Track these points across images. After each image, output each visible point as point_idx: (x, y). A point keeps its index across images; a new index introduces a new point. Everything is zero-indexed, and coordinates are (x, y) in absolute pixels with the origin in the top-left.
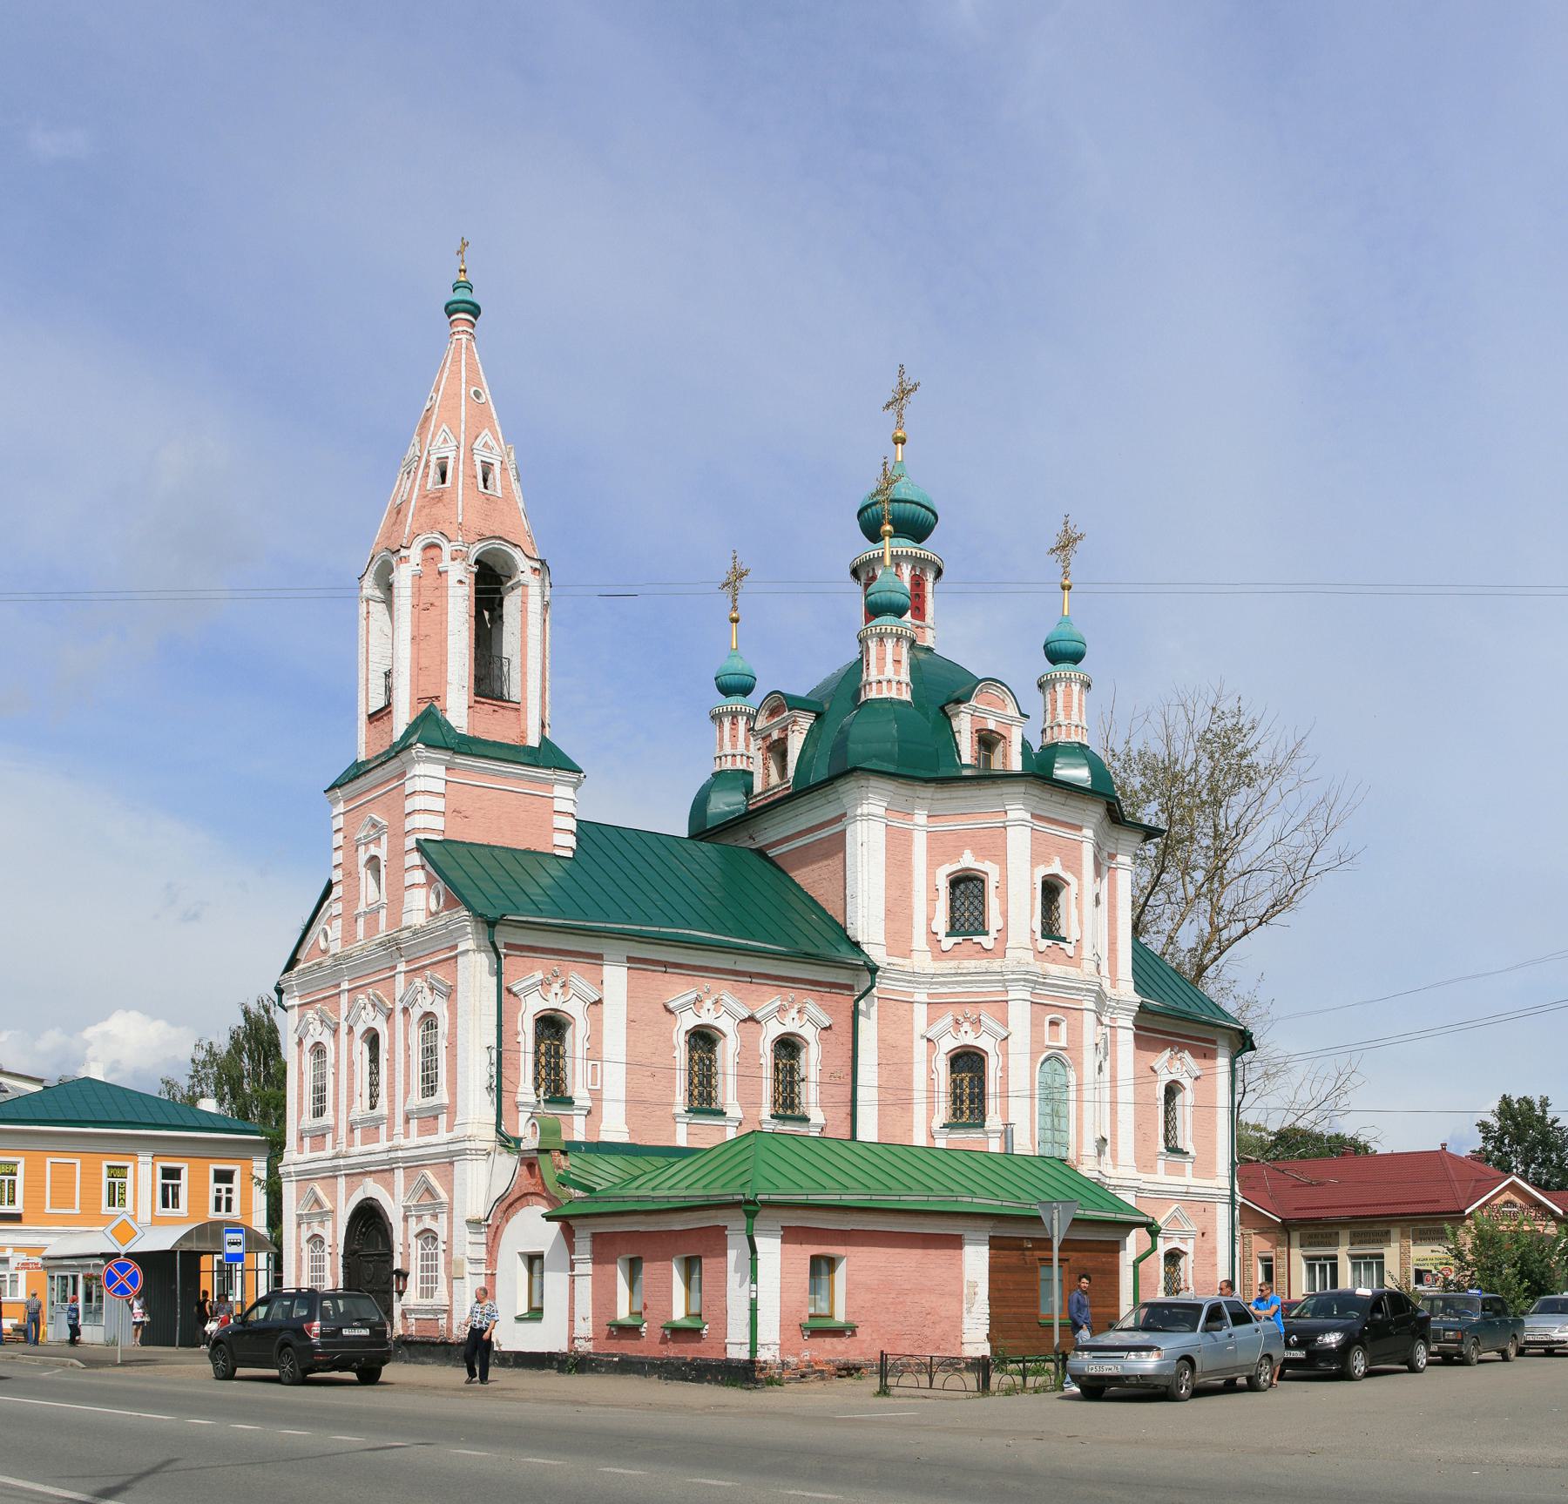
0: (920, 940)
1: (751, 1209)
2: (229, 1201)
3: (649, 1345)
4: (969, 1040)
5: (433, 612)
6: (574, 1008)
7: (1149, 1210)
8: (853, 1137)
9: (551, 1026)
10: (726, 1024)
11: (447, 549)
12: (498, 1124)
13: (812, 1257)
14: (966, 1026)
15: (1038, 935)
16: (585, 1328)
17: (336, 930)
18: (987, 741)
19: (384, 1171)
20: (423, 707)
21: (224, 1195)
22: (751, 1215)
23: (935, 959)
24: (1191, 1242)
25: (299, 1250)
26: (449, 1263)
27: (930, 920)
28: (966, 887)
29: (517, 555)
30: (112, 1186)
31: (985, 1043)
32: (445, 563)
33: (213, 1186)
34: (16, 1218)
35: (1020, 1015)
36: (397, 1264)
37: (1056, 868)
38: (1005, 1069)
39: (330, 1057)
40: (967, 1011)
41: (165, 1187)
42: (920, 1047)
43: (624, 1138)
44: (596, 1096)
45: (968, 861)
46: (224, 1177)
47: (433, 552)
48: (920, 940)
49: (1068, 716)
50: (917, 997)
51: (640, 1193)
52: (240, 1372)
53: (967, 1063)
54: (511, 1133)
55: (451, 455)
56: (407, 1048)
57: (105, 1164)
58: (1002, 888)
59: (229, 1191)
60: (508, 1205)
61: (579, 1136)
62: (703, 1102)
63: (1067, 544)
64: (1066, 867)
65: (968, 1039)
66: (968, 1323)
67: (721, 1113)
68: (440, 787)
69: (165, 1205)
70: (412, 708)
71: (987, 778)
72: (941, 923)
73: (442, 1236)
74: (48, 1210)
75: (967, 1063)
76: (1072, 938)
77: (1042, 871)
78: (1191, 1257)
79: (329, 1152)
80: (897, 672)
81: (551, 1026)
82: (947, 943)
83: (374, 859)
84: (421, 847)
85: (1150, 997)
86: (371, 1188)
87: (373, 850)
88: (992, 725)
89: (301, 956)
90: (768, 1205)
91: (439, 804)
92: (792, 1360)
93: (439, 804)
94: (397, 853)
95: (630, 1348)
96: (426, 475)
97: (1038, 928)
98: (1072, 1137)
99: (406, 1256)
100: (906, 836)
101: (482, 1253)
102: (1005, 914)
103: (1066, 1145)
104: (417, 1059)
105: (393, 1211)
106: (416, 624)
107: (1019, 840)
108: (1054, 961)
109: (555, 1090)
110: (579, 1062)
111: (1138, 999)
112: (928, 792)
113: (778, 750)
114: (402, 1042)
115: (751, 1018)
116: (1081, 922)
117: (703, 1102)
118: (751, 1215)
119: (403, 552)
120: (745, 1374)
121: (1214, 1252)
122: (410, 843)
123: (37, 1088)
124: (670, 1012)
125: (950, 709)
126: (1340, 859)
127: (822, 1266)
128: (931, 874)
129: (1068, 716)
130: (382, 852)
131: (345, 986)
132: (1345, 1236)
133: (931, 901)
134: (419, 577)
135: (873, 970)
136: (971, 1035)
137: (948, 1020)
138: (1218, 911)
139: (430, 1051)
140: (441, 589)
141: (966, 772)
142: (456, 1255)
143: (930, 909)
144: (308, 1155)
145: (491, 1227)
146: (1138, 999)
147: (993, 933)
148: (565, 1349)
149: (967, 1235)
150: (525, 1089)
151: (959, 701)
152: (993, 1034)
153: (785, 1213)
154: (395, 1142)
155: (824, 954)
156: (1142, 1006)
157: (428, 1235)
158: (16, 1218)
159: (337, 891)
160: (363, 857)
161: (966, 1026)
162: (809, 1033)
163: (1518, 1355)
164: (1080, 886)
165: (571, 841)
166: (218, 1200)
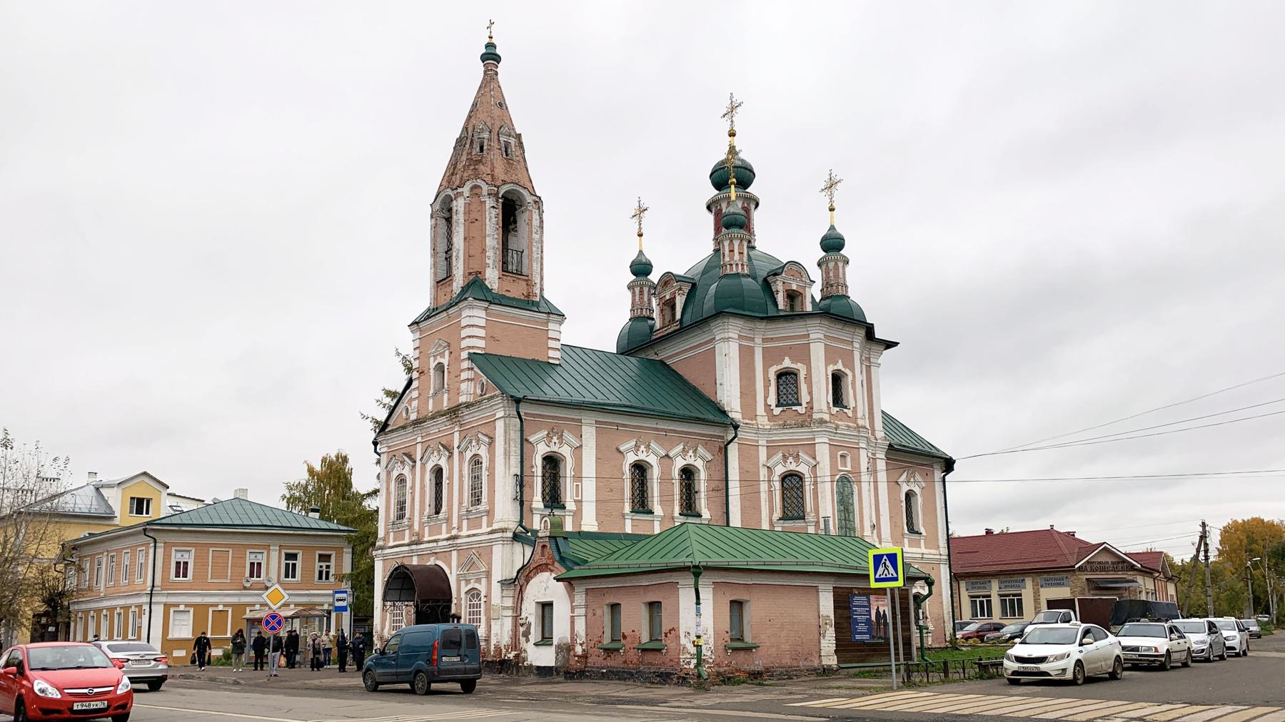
0: (760, 410)
1: (697, 571)
2: (327, 573)
4: (793, 467)
6: (565, 451)
7: (926, 570)
8: (728, 525)
9: (552, 462)
10: (652, 460)
11: (485, 188)
13: (732, 602)
14: (791, 459)
18: (792, 296)
20: (471, 278)
22: (697, 575)
26: (488, 610)
27: (766, 398)
28: (787, 378)
31: (803, 469)
33: (318, 564)
35: (823, 452)
36: (453, 611)
37: (840, 366)
39: (409, 484)
40: (791, 452)
41: (287, 565)
42: (763, 473)
43: (594, 529)
44: (579, 503)
45: (787, 363)
46: (325, 558)
47: (475, 191)
48: (760, 410)
50: (861, 445)
51: (618, 562)
52: (434, 686)
53: (792, 482)
54: (528, 527)
56: (461, 476)
57: (318, 553)
59: (328, 567)
61: (569, 527)
62: (641, 504)
63: (831, 185)
64: (844, 366)
66: (824, 643)
67: (651, 512)
68: (483, 323)
70: (464, 277)
71: (794, 315)
72: (772, 400)
73: (483, 594)
75: (792, 482)
76: (852, 405)
77: (831, 368)
81: (552, 462)
82: (777, 411)
83: (440, 367)
87: (440, 360)
88: (794, 287)
90: (707, 568)
91: (482, 333)
93: (482, 333)
95: (615, 662)
98: (857, 524)
99: (459, 606)
100: (751, 350)
101: (509, 602)
102: (810, 393)
106: (467, 230)
107: (818, 352)
109: (553, 499)
110: (568, 480)
112: (761, 325)
113: (671, 304)
115: (667, 456)
117: (641, 504)
118: (697, 575)
122: (464, 355)
123: (193, 506)
130: (445, 361)
131: (419, 440)
132: (1029, 582)
133: (767, 387)
134: (467, 205)
135: (736, 427)
140: (482, 211)
143: (766, 394)
145: (518, 583)
147: (804, 405)
149: (821, 587)
150: (538, 502)
152: (807, 464)
153: (716, 573)
154: (454, 532)
155: (706, 414)
157: (474, 594)
160: (433, 365)
161: (791, 459)
162: (699, 464)
164: (854, 376)
166: (321, 573)
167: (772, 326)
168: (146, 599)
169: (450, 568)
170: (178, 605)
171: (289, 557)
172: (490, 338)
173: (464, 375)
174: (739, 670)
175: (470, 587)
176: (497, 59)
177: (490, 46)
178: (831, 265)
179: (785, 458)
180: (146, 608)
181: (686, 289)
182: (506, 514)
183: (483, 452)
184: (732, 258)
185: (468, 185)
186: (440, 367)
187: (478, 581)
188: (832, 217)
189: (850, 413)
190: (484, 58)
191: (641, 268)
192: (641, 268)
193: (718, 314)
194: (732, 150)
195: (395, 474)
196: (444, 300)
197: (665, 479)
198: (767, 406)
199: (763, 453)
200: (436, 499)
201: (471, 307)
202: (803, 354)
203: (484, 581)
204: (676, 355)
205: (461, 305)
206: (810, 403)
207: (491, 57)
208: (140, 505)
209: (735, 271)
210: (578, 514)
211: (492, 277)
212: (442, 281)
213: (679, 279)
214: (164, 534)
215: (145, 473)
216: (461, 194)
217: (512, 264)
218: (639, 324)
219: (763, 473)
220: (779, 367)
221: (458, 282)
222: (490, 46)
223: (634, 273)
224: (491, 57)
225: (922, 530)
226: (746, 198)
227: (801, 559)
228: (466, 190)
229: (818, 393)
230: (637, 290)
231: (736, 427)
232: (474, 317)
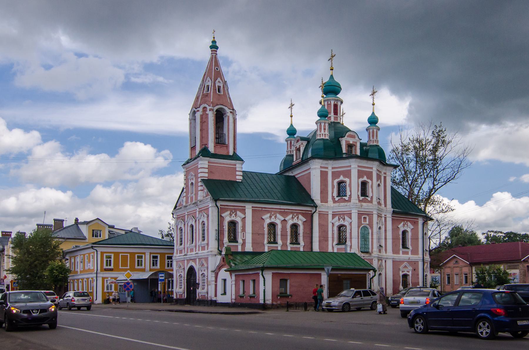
1: (263, 269)
3: (246, 300)
5: (205, 123)
6: (238, 220)
10: (278, 222)
11: (208, 108)
12: (218, 248)
13: (281, 280)
14: (341, 219)
15: (360, 196)
16: (234, 297)
17: (185, 199)
19: (194, 260)
20: (203, 146)
21: (170, 263)
23: (334, 203)
24: (410, 272)
25: (177, 279)
26: (207, 281)
29: (226, 108)
30: (138, 261)
31: (346, 223)
32: (208, 112)
33: (167, 261)
34: (111, 270)
36: (197, 282)
37: (365, 178)
38: (351, 230)
39: (206, 225)
41: (153, 260)
45: (342, 178)
49: (373, 138)
55: (210, 85)
56: (199, 230)
57: (166, 255)
58: (350, 185)
59: (171, 261)
60: (219, 268)
61: (240, 249)
64: (368, 178)
65: (342, 222)
69: (153, 265)
72: (335, 194)
74: (120, 267)
76: (371, 195)
77: (361, 180)
78: (410, 276)
79: (183, 254)
80: (325, 132)
81: (233, 224)
82: (337, 199)
83: (192, 184)
84: (203, 180)
85: (397, 209)
86: (192, 263)
88: (351, 142)
89: (178, 205)
92: (274, 303)
94: (197, 182)
96: (204, 89)
97: (360, 193)
102: (351, 191)
103: (369, 248)
104: (201, 232)
105: (196, 268)
108: (365, 202)
109: (233, 239)
111: (392, 210)
113: (298, 150)
114: (198, 228)
115: (285, 220)
116: (372, 192)
119: (198, 109)
120: (264, 307)
121: (418, 275)
122: (199, 180)
124: (263, 219)
125: (340, 139)
126: (467, 166)
127: (283, 282)
128: (333, 182)
129: (373, 138)
130: (194, 182)
137: (337, 218)
138: (435, 180)
139: (204, 230)
141: (344, 156)
142: (209, 279)
143: (332, 191)
144: (179, 255)
146: (392, 210)
148: (230, 302)
151: (342, 137)
154: (186, 253)
156: (393, 211)
158: (111, 270)
159: (185, 190)
160: (190, 183)
161: (341, 219)
163: (132, 301)
164: (372, 183)
165: (241, 178)
166: (168, 264)
168: (95, 275)
170: (108, 278)
171: (154, 257)
172: (210, 172)
173: (200, 188)
174: (247, 305)
176: (217, 48)
177: (214, 42)
178: (371, 131)
180: (95, 279)
181: (305, 143)
182: (213, 244)
183: (205, 220)
186: (192, 184)
187: (408, 272)
188: (373, 108)
189: (369, 199)
190: (211, 47)
193: (313, 158)
195: (179, 227)
196: (194, 157)
197: (284, 228)
198: (333, 197)
199: (330, 217)
201: (201, 160)
202: (348, 174)
203: (206, 270)
204: (296, 173)
205: (199, 159)
206: (350, 195)
208: (95, 234)
209: (322, 137)
210: (244, 244)
211: (211, 148)
212: (193, 148)
214: (100, 248)
215: (98, 219)
216: (198, 111)
217: (220, 139)
218: (288, 157)
219: (330, 225)
221: (198, 149)
222: (214, 42)
223: (288, 134)
225: (410, 247)
228: (201, 109)
229: (354, 190)
230: (289, 142)
231: (316, 207)
232: (203, 163)
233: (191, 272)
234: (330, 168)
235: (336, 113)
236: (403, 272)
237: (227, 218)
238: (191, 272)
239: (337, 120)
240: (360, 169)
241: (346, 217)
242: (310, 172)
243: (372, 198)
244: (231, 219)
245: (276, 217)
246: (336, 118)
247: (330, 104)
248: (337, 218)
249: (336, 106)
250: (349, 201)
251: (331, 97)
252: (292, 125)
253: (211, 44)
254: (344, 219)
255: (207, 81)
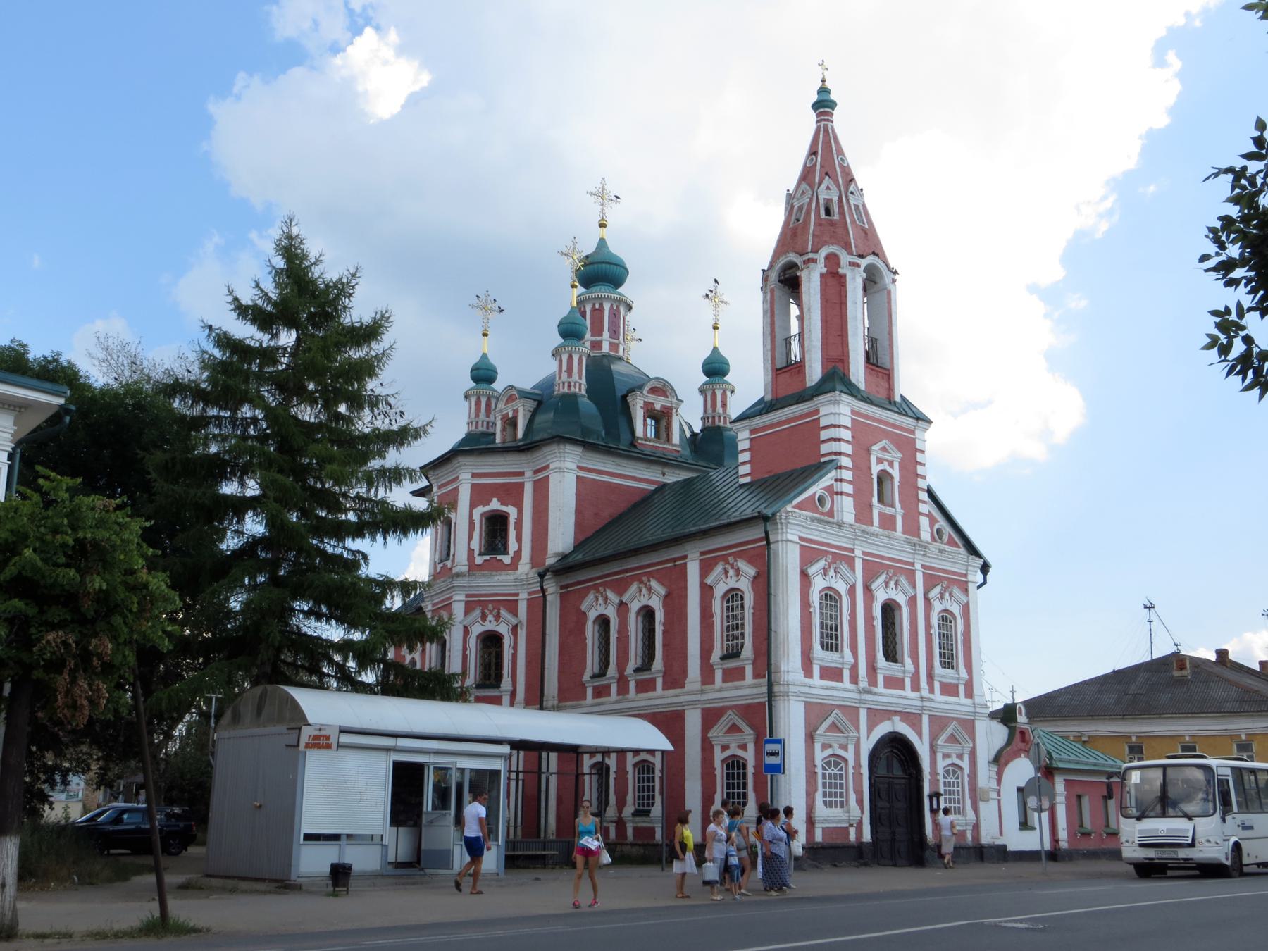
11: (845, 258)
14: (490, 617)
31: (503, 629)
36: (927, 790)
39: (507, 642)
45: (495, 505)
65: (490, 625)
72: (475, 545)
136: (494, 623)
137: (477, 613)
161: (490, 617)
167: (591, 455)
169: (920, 734)
175: (728, 753)
176: (832, 105)
177: (823, 90)
179: (484, 617)
181: (531, 405)
184: (570, 375)
185: (824, 252)
187: (844, 747)
190: (816, 106)
191: (483, 374)
192: (483, 374)
194: (602, 242)
198: (471, 551)
200: (768, 595)
207: (824, 105)
213: (524, 395)
220: (487, 508)
222: (823, 90)
224: (824, 105)
226: (615, 300)
227: (1073, 757)
233: (1141, 845)
234: (528, 474)
235: (614, 333)
236: (946, 756)
237: (881, 597)
238: (1141, 845)
239: (617, 351)
240: (477, 481)
241: (503, 612)
242: (457, 489)
243: (518, 554)
244: (483, 629)
245: (498, 617)
246: (614, 346)
247: (601, 310)
248: (477, 613)
249: (615, 315)
250: (514, 565)
251: (601, 291)
252: (715, 349)
253: (815, 98)
254: (498, 617)
255: (823, 186)
